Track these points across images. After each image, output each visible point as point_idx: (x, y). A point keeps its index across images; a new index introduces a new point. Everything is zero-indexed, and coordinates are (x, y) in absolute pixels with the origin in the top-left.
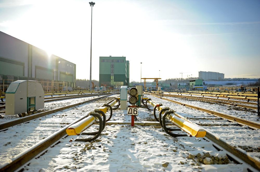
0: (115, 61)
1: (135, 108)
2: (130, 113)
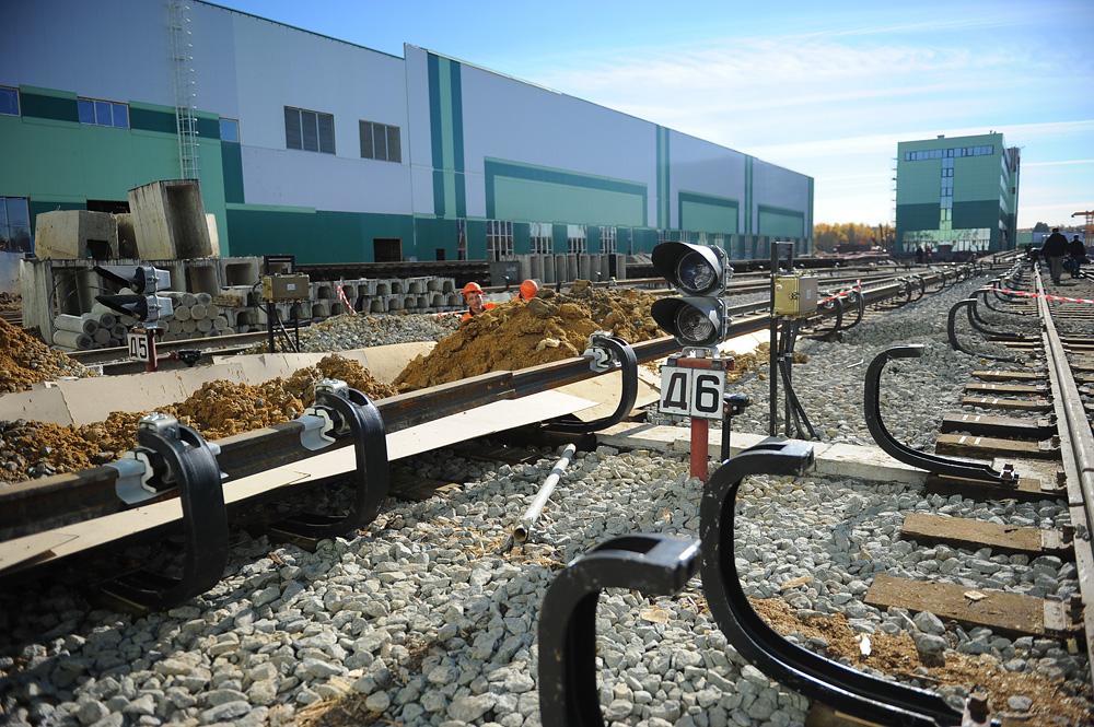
1: (705, 372)
2: (675, 404)
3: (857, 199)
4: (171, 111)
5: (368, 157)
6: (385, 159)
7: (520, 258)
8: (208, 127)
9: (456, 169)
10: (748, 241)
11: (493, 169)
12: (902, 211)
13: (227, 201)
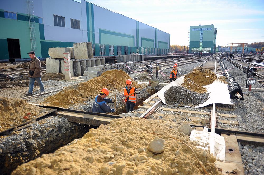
0: (204, 29)
3: (181, 40)
4: (27, 16)
5: (73, 28)
6: (77, 29)
7: (123, 55)
8: (36, 20)
9: (93, 31)
10: (156, 49)
11: (101, 31)
12: (191, 43)
13: (41, 39)
